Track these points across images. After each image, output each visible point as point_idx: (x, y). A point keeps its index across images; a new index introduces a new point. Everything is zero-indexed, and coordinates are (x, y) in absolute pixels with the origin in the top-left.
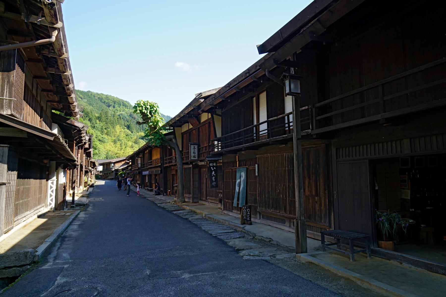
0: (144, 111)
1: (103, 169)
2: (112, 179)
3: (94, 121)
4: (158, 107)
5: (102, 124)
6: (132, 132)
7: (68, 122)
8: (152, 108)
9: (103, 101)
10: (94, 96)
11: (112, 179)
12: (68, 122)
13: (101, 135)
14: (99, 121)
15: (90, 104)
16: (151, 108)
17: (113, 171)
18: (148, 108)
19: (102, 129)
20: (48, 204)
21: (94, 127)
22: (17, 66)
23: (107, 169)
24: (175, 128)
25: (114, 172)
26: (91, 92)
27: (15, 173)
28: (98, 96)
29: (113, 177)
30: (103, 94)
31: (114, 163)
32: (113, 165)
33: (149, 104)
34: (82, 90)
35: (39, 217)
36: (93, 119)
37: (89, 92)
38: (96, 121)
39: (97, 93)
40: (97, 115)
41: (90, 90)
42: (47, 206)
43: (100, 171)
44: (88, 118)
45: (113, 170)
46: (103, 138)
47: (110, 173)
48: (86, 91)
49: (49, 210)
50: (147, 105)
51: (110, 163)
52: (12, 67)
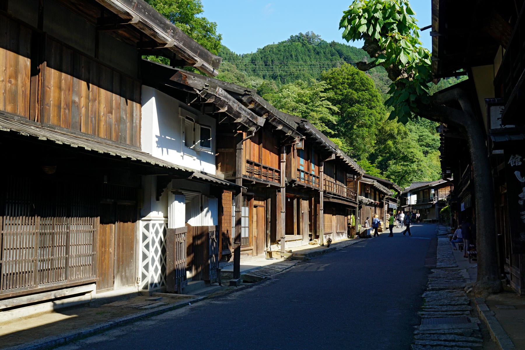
0: (377, 36)
1: (418, 201)
2: (434, 221)
4: (409, 12)
6: (256, 65)
7: (174, 78)
8: (391, 15)
11: (434, 221)
12: (174, 78)
13: (430, 135)
16: (385, 18)
17: (434, 206)
18: (377, 20)
20: (140, 276)
23: (423, 201)
24: (475, 70)
25: (437, 207)
29: (435, 219)
31: (437, 188)
32: (433, 192)
33: (380, 6)
35: (57, 310)
42: (127, 280)
43: (413, 205)
45: (435, 202)
46: (433, 140)
47: (429, 210)
49: (140, 289)
50: (376, 11)
51: (429, 188)
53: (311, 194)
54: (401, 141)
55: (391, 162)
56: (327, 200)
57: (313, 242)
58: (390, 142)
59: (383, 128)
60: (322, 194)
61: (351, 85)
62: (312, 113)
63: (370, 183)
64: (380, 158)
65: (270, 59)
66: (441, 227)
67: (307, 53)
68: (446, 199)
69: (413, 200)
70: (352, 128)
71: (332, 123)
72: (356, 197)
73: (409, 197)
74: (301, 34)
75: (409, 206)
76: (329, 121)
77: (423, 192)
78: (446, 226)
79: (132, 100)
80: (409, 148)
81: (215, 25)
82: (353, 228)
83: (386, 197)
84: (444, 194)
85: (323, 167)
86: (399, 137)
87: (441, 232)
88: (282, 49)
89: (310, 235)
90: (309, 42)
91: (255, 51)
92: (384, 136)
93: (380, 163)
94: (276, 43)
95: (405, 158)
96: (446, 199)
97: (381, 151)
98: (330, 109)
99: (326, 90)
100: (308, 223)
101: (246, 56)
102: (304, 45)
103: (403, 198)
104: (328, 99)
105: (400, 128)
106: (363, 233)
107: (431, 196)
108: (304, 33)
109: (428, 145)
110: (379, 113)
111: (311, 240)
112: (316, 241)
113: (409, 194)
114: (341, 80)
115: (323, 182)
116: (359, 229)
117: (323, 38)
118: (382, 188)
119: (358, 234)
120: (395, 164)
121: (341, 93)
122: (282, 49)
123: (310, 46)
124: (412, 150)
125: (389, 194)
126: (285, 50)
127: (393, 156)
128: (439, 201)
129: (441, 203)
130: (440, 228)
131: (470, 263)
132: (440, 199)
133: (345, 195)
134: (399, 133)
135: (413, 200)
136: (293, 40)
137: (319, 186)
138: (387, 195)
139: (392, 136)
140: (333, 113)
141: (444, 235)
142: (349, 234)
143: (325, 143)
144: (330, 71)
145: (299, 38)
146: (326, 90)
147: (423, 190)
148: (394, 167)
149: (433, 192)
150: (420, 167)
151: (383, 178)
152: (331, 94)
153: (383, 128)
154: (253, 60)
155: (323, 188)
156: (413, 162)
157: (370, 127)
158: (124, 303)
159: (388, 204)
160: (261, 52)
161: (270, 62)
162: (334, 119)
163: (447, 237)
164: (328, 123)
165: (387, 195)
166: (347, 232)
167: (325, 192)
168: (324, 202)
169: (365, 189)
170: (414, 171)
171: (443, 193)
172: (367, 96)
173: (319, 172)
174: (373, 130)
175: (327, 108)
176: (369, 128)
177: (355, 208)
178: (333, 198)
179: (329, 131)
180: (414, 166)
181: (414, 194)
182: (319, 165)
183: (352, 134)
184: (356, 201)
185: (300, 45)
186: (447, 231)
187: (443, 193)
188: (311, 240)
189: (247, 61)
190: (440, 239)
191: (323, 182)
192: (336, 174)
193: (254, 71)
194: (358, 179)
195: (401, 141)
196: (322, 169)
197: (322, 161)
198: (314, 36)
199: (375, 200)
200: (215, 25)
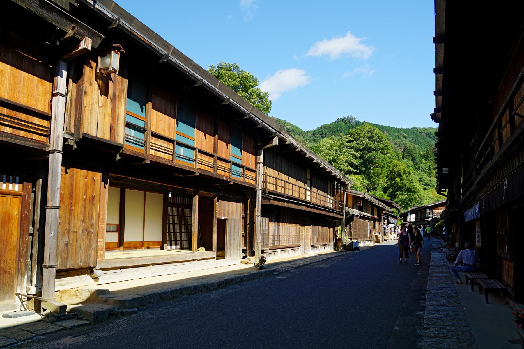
1: (416, 218)
3: (418, 161)
5: (429, 164)
9: (432, 136)
10: (421, 133)
13: (428, 177)
14: (426, 160)
15: (416, 143)
19: (429, 169)
21: (419, 167)
22: (80, 48)
23: (421, 218)
25: (431, 223)
26: (417, 128)
27: (268, 219)
28: (426, 132)
30: (431, 128)
31: (432, 208)
32: (428, 211)
34: (405, 128)
36: (417, 157)
37: (414, 128)
38: (421, 161)
39: (424, 128)
40: (422, 153)
41: (417, 126)
44: (410, 158)
45: (430, 219)
46: (430, 181)
48: (410, 128)
51: (425, 208)
52: (85, 51)
53: (242, 193)
54: (406, 178)
55: (399, 193)
56: (266, 203)
57: (246, 260)
58: (398, 179)
59: (393, 169)
60: (259, 194)
61: (370, 138)
62: (340, 157)
63: (361, 196)
64: (391, 190)
65: (324, 133)
66: (435, 240)
67: (348, 129)
68: (439, 217)
69: (412, 218)
70: (370, 168)
71: (355, 165)
72: (342, 209)
73: (409, 216)
74: (344, 117)
75: (410, 222)
76: (352, 163)
77: (420, 212)
78: (439, 239)
79: (281, 172)
80: (412, 183)
81: (267, 94)
82: (340, 239)
83: (384, 212)
84: (437, 213)
85: (261, 157)
86: (404, 176)
87: (435, 245)
88: (332, 126)
89: (244, 251)
90: (349, 122)
91: (315, 129)
92: (393, 175)
93: (390, 193)
94: (329, 123)
95: (409, 190)
96: (439, 217)
97: (391, 186)
98: (353, 154)
99: (350, 141)
100: (242, 232)
101: (310, 132)
102: (346, 124)
103: (404, 217)
104: (352, 148)
105: (406, 169)
106: (348, 245)
107: (427, 214)
108: (346, 117)
109: (426, 184)
110: (390, 158)
111: (244, 257)
112: (250, 260)
113: (409, 214)
114: (362, 135)
115: (261, 178)
116: (345, 241)
117: (358, 119)
118: (382, 205)
119: (343, 246)
120: (402, 194)
121: (362, 143)
122: (332, 126)
123: (350, 125)
124: (414, 184)
125: (387, 210)
126: (334, 128)
127: (400, 188)
128: (433, 219)
129: (436, 220)
130: (434, 240)
131: (487, 302)
132: (434, 217)
133: (331, 206)
134: (404, 173)
135: (412, 218)
136: (339, 121)
137: (256, 183)
138: (385, 210)
139: (399, 175)
140: (356, 158)
141: (439, 250)
142: (336, 246)
143: (228, 99)
144: (354, 129)
145: (343, 120)
146: (350, 141)
147: (420, 210)
148: (400, 196)
149: (428, 211)
150: (420, 196)
151: (387, 198)
152: (353, 144)
153: (393, 169)
154: (314, 133)
155: (261, 185)
156: (414, 193)
157: (383, 167)
158: (287, 265)
159: (388, 220)
160: (319, 129)
161: (324, 135)
162: (356, 162)
163: (441, 252)
164: (352, 165)
165: (385, 210)
166: (332, 244)
167: (264, 191)
168: (263, 206)
169: (357, 202)
170: (416, 199)
171: (437, 212)
172: (382, 146)
173: (257, 163)
174: (385, 169)
175: (351, 154)
176: (382, 168)
177: (342, 219)
178: (275, 199)
179: (352, 170)
180: (415, 195)
181: (413, 213)
182: (257, 154)
183: (370, 172)
184: (342, 212)
185: (344, 124)
186: (440, 244)
187: (437, 212)
188: (244, 257)
189: (310, 134)
190: (433, 255)
191: (261, 178)
192: (311, 180)
193: (314, 140)
194: (344, 190)
195: (406, 178)
196: (261, 158)
197: (260, 148)
198: (352, 119)
199: (372, 214)
200: (267, 94)
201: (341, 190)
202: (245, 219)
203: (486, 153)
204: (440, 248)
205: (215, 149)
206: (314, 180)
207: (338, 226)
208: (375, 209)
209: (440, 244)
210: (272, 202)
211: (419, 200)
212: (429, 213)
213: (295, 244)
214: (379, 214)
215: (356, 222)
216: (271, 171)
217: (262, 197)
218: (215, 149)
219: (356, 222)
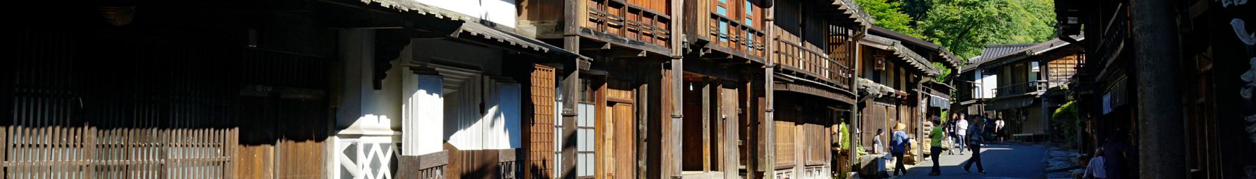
1: (1000, 89)
23: (1013, 91)
25: (1045, 104)
31: (1045, 59)
32: (1035, 68)
45: (1040, 93)
56: (782, 88)
60: (769, 73)
63: (885, 48)
66: (1055, 153)
69: (987, 87)
72: (851, 82)
73: (978, 81)
75: (980, 101)
77: (1012, 69)
78: (1067, 149)
82: (845, 154)
83: (924, 80)
84: (1062, 73)
87: (1055, 165)
96: (1066, 86)
100: (738, 141)
103: (963, 84)
107: (1032, 78)
113: (978, 74)
115: (772, 46)
116: (858, 156)
118: (913, 59)
119: (856, 168)
128: (1049, 91)
129: (1056, 96)
132: (1052, 85)
135: (987, 87)
137: (764, 54)
138: (926, 75)
147: (1012, 65)
149: (1035, 68)
150: (1004, 10)
151: (917, 36)
155: (773, 59)
159: (929, 98)
165: (926, 75)
166: (829, 164)
167: (777, 68)
169: (873, 62)
170: (991, 20)
171: (1061, 71)
173: (764, 20)
177: (849, 106)
178: (797, 82)
181: (990, 73)
184: (851, 89)
186: (1069, 160)
187: (1061, 71)
191: (772, 46)
194: (855, 39)
199: (897, 87)
201: (847, 36)
202: (742, 117)
203: (1099, 77)
204: (1066, 170)
205: (738, 14)
206: (810, 25)
207: (839, 123)
208: (902, 71)
209: (1069, 160)
210: (793, 88)
211: (1003, 22)
212: (1039, 75)
213: (790, 163)
214: (909, 87)
215: (868, 112)
216: (786, 36)
217: (775, 79)
218: (738, 14)
219: (868, 112)
